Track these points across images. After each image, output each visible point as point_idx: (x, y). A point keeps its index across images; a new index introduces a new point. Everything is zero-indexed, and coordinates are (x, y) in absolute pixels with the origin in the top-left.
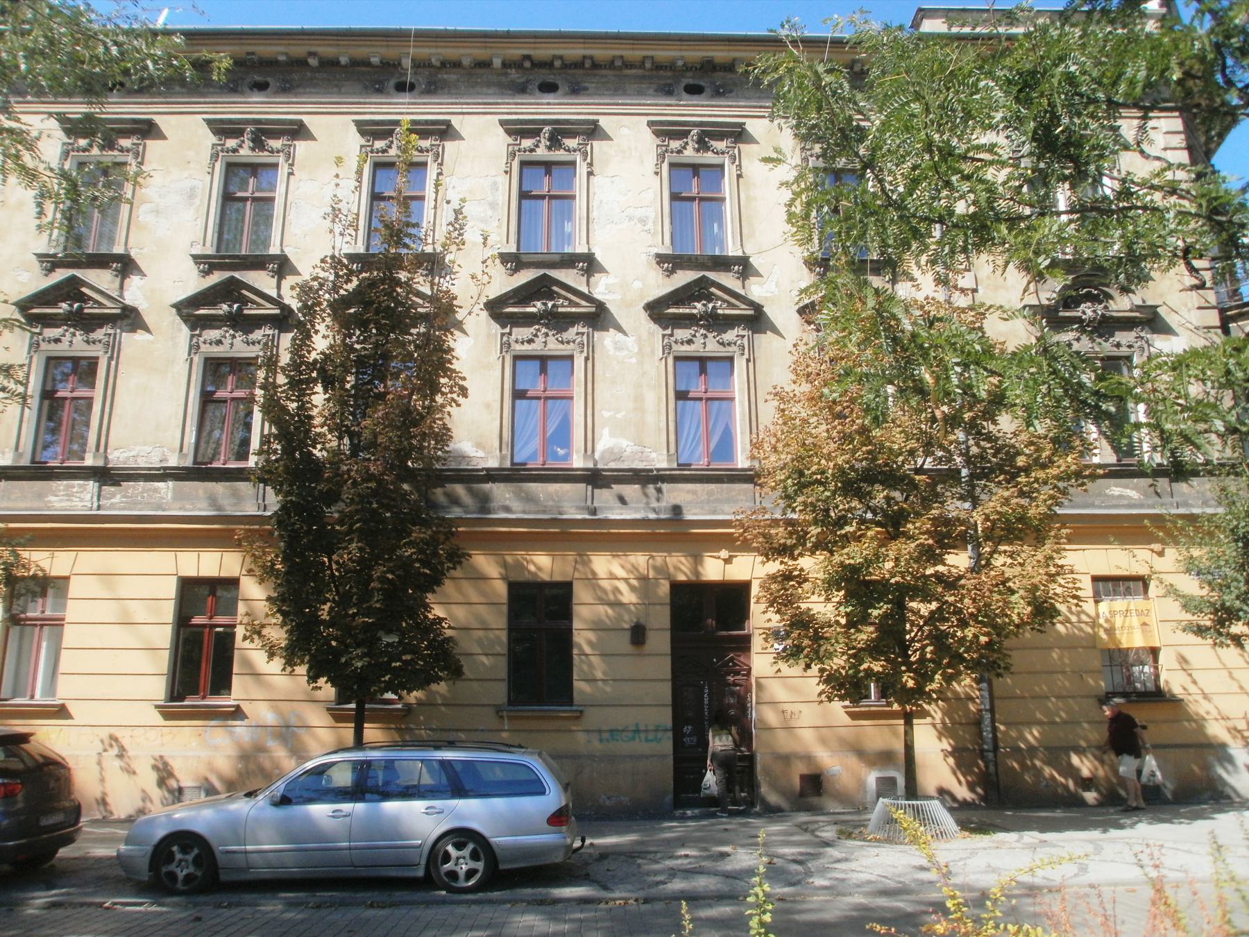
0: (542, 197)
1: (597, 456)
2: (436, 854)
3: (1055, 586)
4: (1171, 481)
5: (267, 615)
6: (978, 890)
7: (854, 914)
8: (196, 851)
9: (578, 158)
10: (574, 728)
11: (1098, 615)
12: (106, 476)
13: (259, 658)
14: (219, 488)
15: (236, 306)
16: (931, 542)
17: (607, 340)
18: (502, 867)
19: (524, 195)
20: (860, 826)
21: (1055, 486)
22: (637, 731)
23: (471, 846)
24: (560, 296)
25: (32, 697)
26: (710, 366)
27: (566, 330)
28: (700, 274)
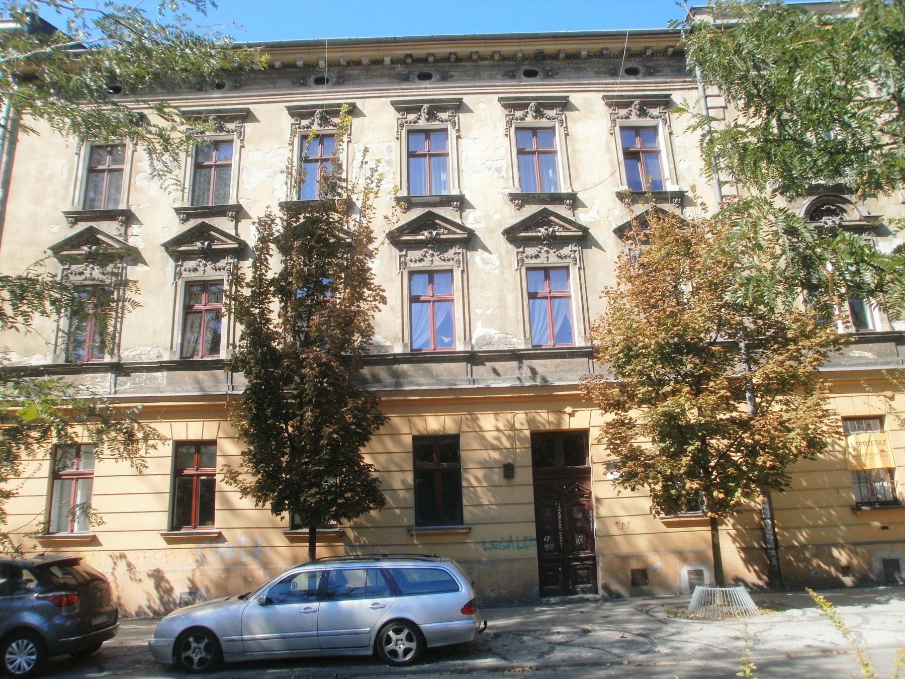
0: (424, 156)
1: (473, 342)
2: (381, 638)
3: (823, 425)
4: (897, 345)
5: (242, 465)
6: (784, 653)
7: (697, 673)
8: (206, 641)
9: (449, 126)
10: (468, 541)
11: (847, 446)
12: (120, 369)
13: (235, 497)
14: (201, 374)
15: (206, 243)
16: (729, 394)
17: (477, 257)
18: (429, 646)
19: (411, 155)
20: (682, 607)
21: (818, 351)
22: (511, 541)
23: (406, 631)
24: (441, 227)
25: (72, 531)
26: (552, 273)
27: (446, 251)
28: (543, 207)
